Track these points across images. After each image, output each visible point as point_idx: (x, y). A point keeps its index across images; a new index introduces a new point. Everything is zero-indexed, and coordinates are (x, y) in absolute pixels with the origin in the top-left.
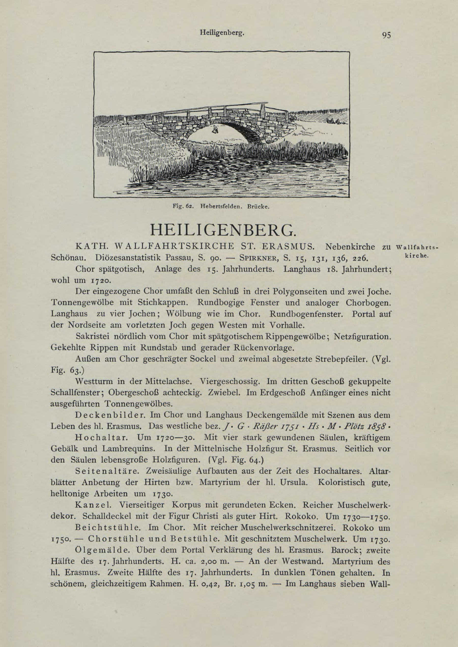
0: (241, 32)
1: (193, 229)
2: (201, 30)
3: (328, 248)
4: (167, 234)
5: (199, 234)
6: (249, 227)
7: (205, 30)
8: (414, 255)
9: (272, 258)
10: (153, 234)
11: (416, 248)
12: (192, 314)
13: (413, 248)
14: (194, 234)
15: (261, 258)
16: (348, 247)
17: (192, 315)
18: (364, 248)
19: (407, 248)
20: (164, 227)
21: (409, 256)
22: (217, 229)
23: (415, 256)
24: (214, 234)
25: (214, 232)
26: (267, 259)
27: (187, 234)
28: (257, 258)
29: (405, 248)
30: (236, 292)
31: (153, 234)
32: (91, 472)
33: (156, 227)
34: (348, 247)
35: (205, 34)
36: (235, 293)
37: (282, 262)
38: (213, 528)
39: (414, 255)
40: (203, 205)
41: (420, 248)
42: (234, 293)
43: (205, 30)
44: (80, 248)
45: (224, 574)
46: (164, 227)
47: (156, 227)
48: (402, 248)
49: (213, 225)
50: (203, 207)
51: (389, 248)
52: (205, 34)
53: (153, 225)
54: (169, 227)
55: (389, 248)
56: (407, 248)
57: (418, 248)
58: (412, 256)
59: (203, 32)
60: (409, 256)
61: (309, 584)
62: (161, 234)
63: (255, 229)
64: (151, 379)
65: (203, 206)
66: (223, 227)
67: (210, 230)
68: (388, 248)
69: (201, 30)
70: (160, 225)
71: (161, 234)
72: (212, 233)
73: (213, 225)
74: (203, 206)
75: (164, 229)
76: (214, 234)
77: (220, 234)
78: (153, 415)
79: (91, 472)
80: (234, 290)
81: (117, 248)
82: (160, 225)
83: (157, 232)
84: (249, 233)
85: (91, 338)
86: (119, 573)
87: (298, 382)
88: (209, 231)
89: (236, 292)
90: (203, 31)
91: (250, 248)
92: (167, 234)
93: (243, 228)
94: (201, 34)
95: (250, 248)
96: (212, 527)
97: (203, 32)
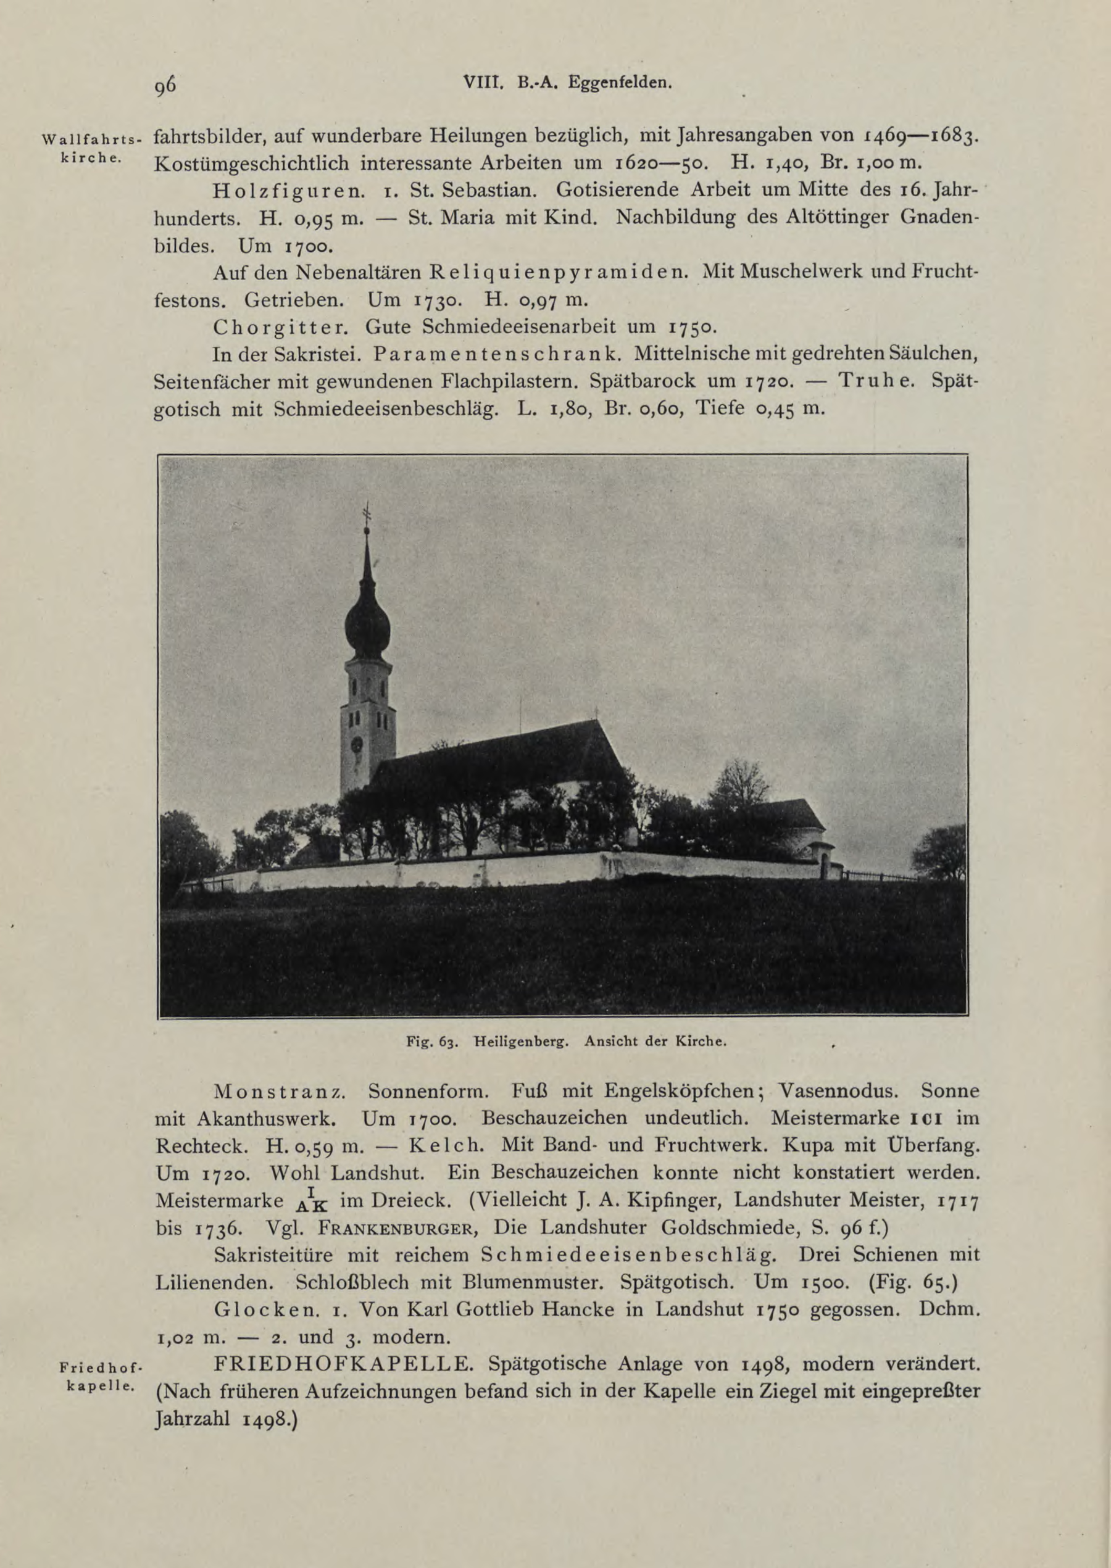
0: (491, 407)
8: (82, 157)
11: (89, 140)
12: (338, 136)
13: (82, 141)
17: (338, 139)
19: (68, 141)
21: (70, 159)
23: (85, 160)
29: (63, 142)
30: (542, 1093)
32: (297, 329)
36: (539, 1096)
37: (918, 1292)
38: (402, 1257)
39: (82, 157)
40: (480, 1039)
41: (100, 140)
42: (536, 1094)
44: (362, 1369)
45: (406, 1395)
48: (57, 141)
50: (480, 1044)
56: (68, 141)
57: (95, 142)
58: (78, 159)
60: (70, 159)
61: (745, 136)
65: (480, 1041)
74: (480, 1041)
79: (297, 329)
80: (536, 1087)
81: (276, 1177)
85: (312, 360)
86: (299, 1119)
87: (672, 355)
89: (542, 1093)
96: (398, 1254)
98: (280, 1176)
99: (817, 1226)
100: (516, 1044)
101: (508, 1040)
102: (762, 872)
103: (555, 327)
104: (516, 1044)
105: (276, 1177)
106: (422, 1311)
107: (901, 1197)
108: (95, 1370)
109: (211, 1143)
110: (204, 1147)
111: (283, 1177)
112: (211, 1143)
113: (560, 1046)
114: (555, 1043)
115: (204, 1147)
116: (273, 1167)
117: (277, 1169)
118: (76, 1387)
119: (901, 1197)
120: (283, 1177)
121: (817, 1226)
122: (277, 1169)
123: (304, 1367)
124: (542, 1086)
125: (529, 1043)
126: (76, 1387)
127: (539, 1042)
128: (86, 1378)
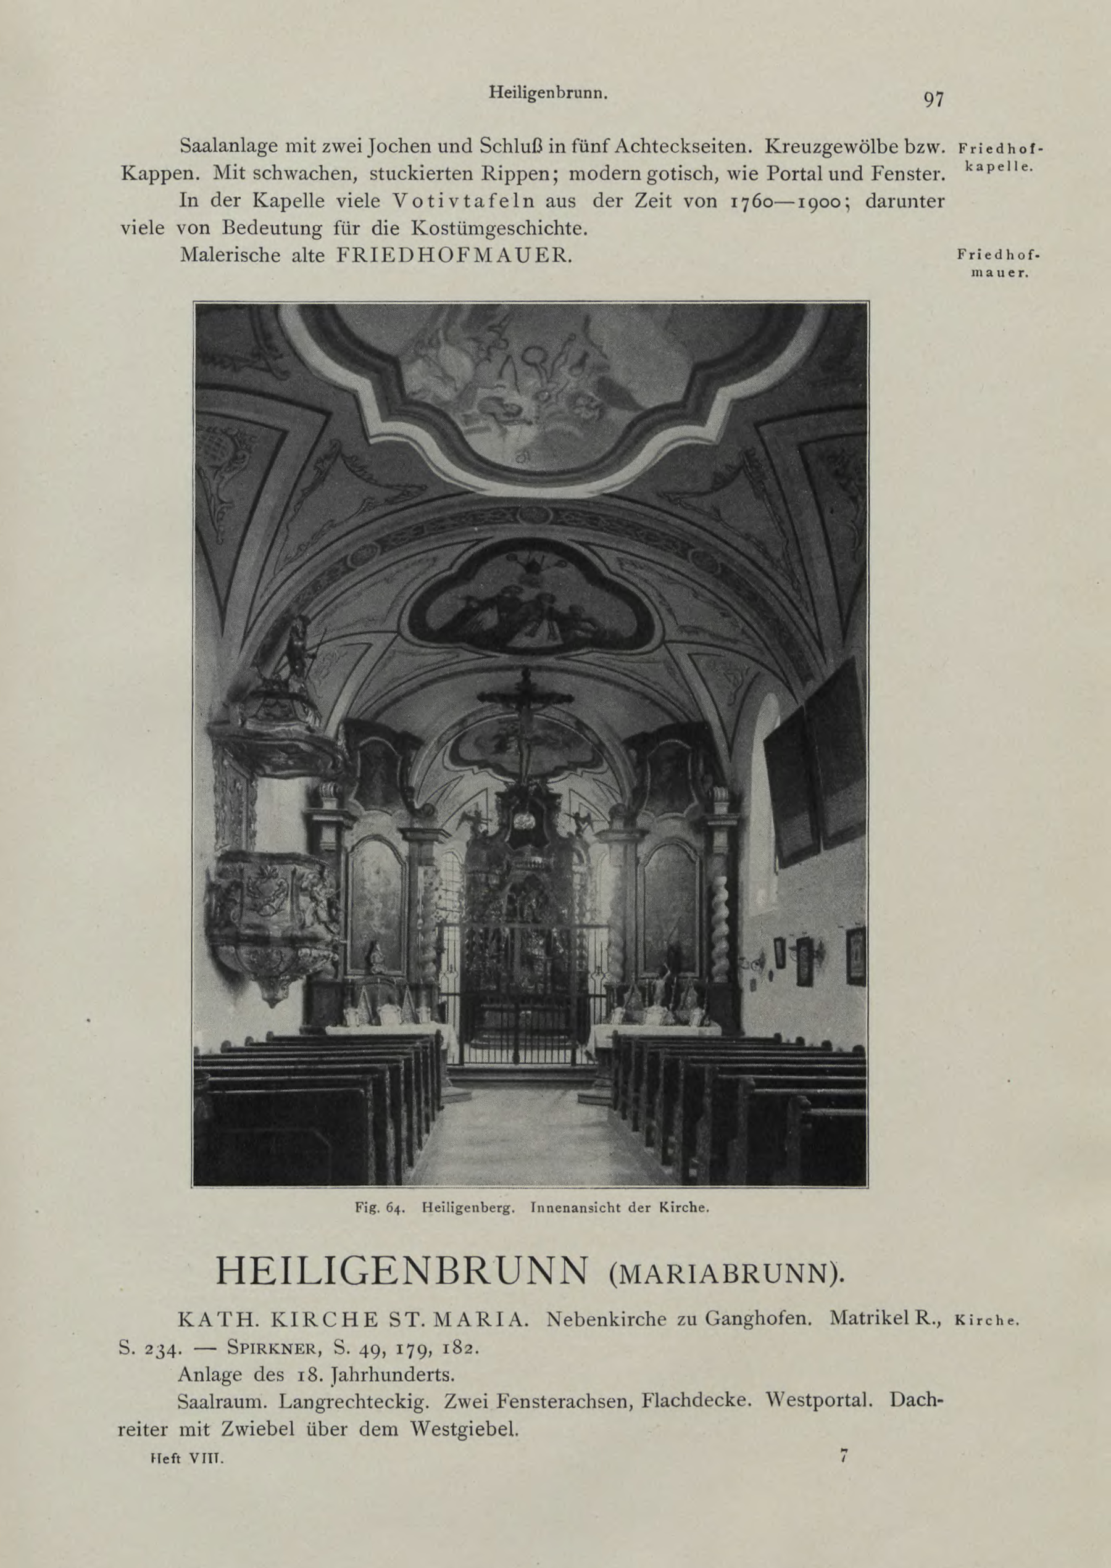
1: (316, 1269)
2: (492, 87)
3: (553, 1322)
4: (256, 1282)
5: (330, 1282)
6: (448, 1264)
7: (501, 87)
9: (305, 1349)
10: (221, 1281)
14: (319, 1282)
15: (280, 1349)
16: (603, 1321)
18: (641, 1321)
20: (248, 1265)
22: (370, 1267)
24: (363, 1281)
25: (364, 1276)
26: (294, 1350)
27: (302, 1282)
28: (267, 1349)
31: (221, 1281)
33: (231, 1263)
34: (603, 1321)
35: (500, 96)
42: (531, 149)
43: (501, 87)
46: (248, 1265)
47: (231, 1263)
49: (363, 1258)
51: (692, 1321)
52: (500, 96)
53: (221, 1259)
54: (262, 1264)
55: (692, 1321)
59: (497, 92)
62: (240, 1282)
63: (462, 1269)
64: (228, 166)
65: (427, 1207)
66: (384, 1263)
67: (354, 1270)
68: (692, 1322)
69: (492, 87)
70: (240, 1259)
71: (240, 1282)
72: (360, 1278)
73: (363, 1258)
74: (427, 1207)
75: (250, 1270)
76: (363, 1281)
77: (377, 1282)
78: (222, 173)
81: (417, 1433)
82: (240, 1259)
83: (231, 1277)
84: (449, 1276)
88: (353, 1273)
90: (496, 89)
91: (412, 1325)
92: (256, 1282)
93: (434, 1264)
94: (492, 96)
95: (412, 1325)
97: (497, 92)
98: (420, 1431)
99: (339, 1346)
100: (463, 1210)
101: (455, 1205)
102: (554, 238)
103: (525, 1403)
104: (463, 1210)
105: (417, 1433)
106: (136, 175)
107: (547, 1398)
108: (994, 150)
109: (374, 1398)
110: (367, 1403)
111: (424, 1432)
112: (374, 1398)
113: (506, 1212)
114: (501, 1209)
115: (367, 1403)
116: (414, 1423)
117: (418, 1425)
118: (974, 167)
119: (547, 1398)
120: (424, 1432)
121: (339, 1346)
122: (418, 1425)
123: (426, 258)
124: (538, 142)
125: (475, 1209)
126: (974, 167)
127: (485, 1208)
128: (985, 159)
